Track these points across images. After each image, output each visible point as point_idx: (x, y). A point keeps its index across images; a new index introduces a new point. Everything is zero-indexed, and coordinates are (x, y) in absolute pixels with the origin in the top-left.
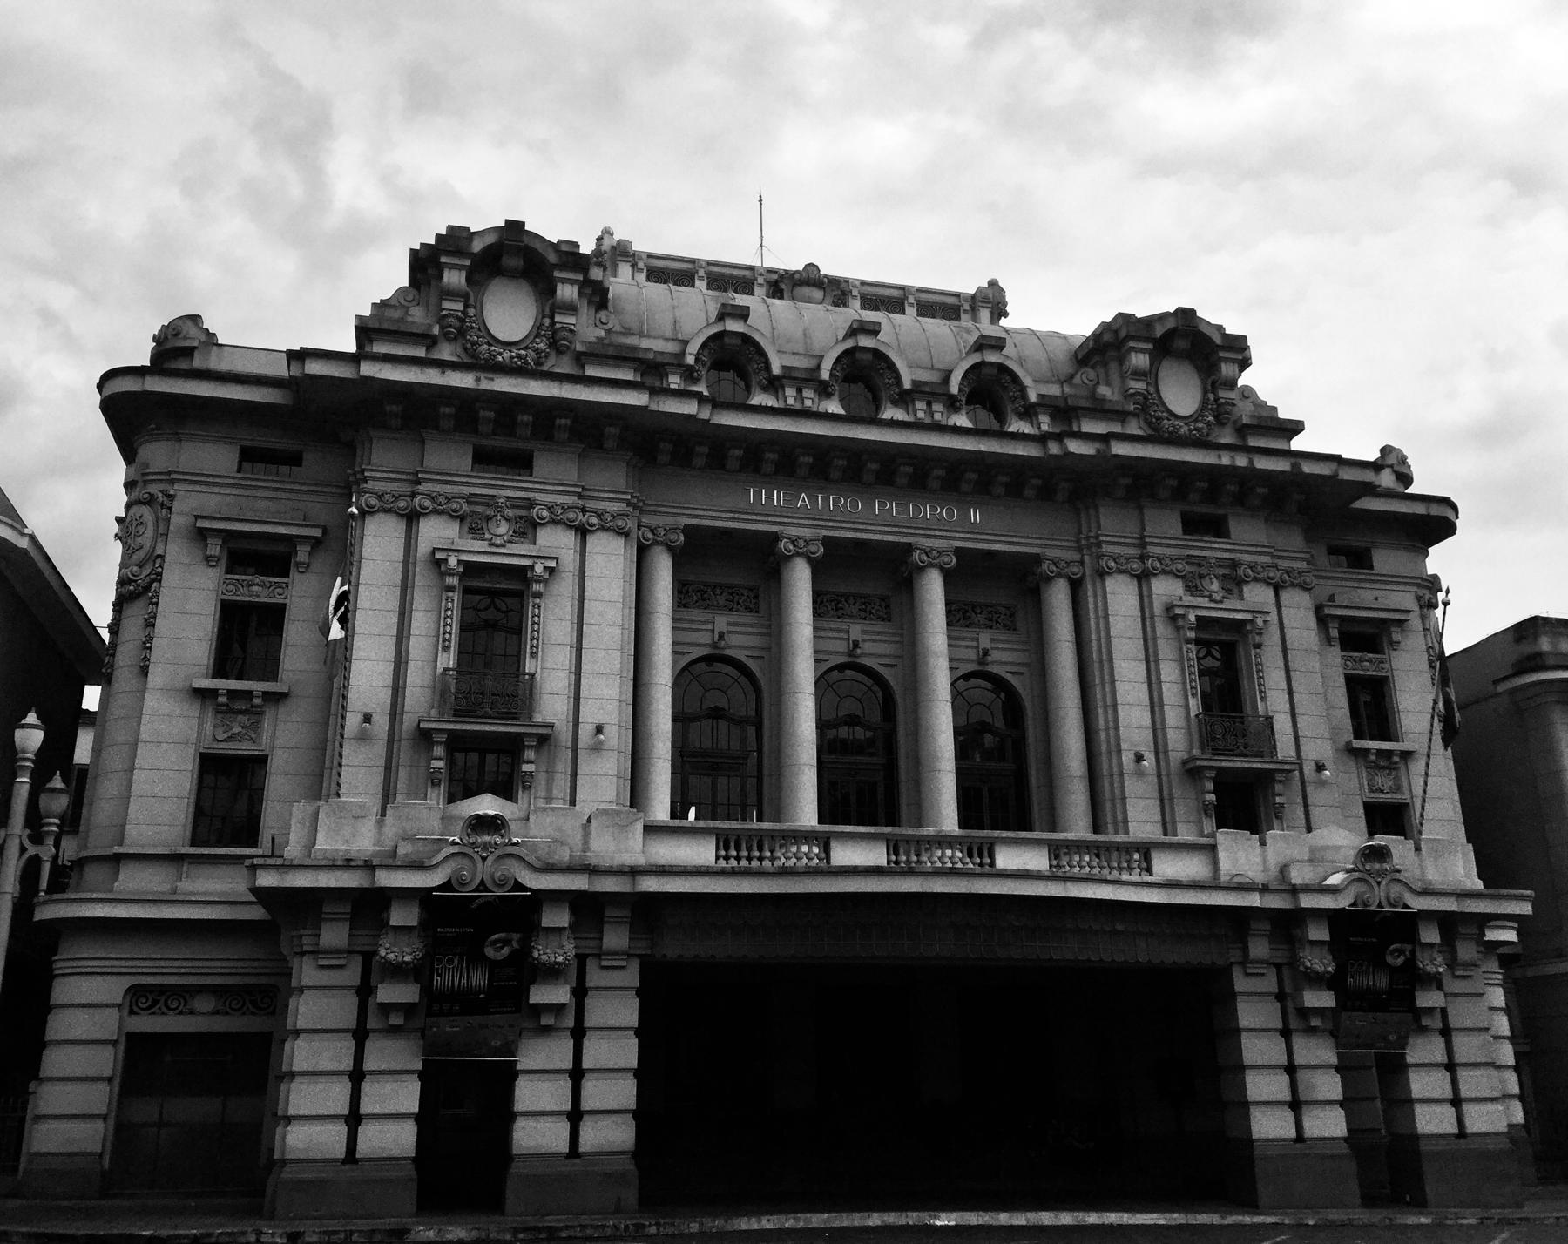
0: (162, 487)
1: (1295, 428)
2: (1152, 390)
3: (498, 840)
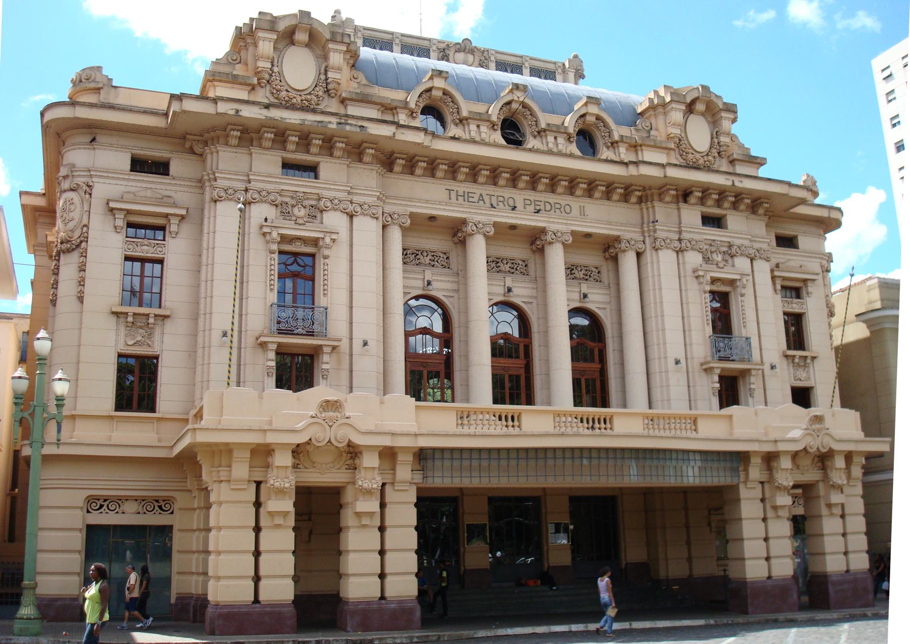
1: (759, 162)
2: (683, 135)
3: (339, 415)
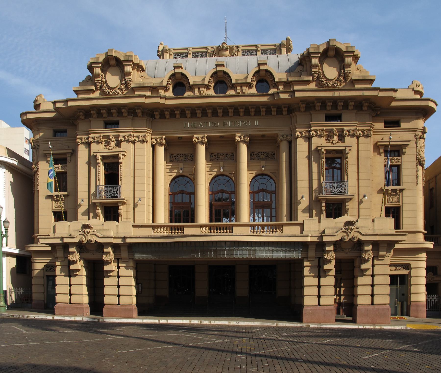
0: (37, 143)
2: (320, 71)
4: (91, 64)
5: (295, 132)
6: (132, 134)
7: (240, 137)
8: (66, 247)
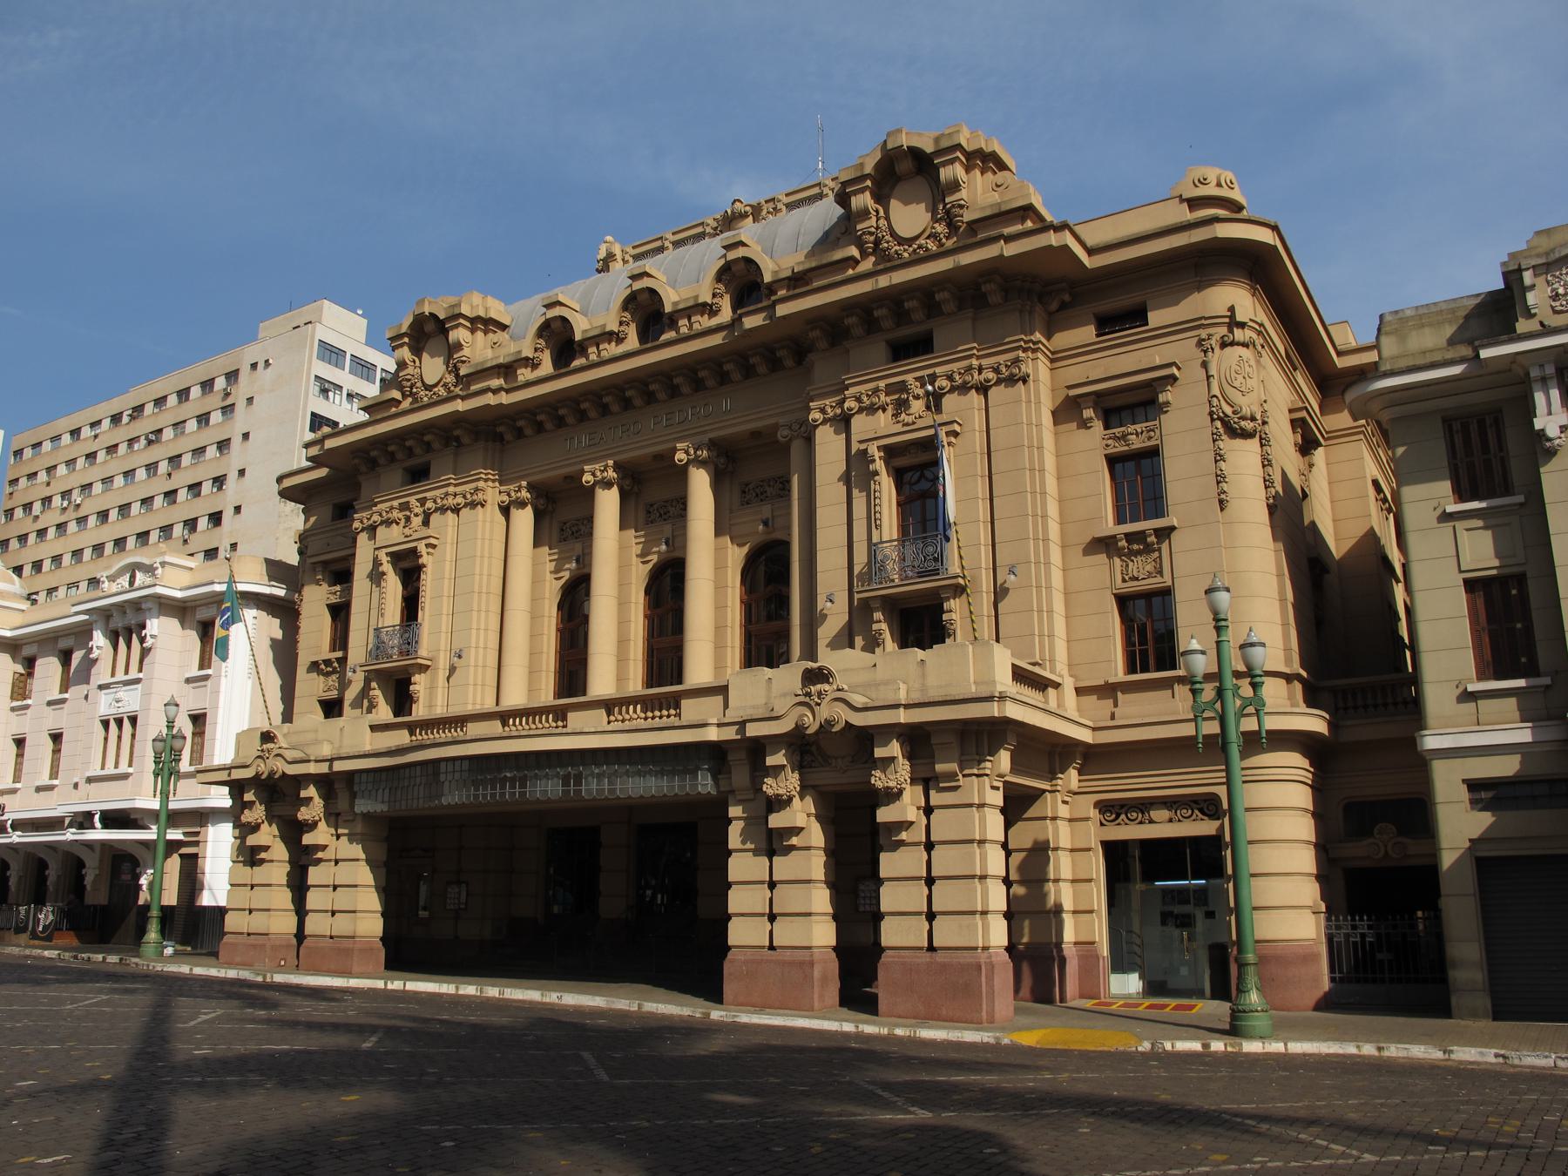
4: (845, 184)
5: (809, 410)
6: (975, 362)
7: (687, 453)
8: (756, 749)
